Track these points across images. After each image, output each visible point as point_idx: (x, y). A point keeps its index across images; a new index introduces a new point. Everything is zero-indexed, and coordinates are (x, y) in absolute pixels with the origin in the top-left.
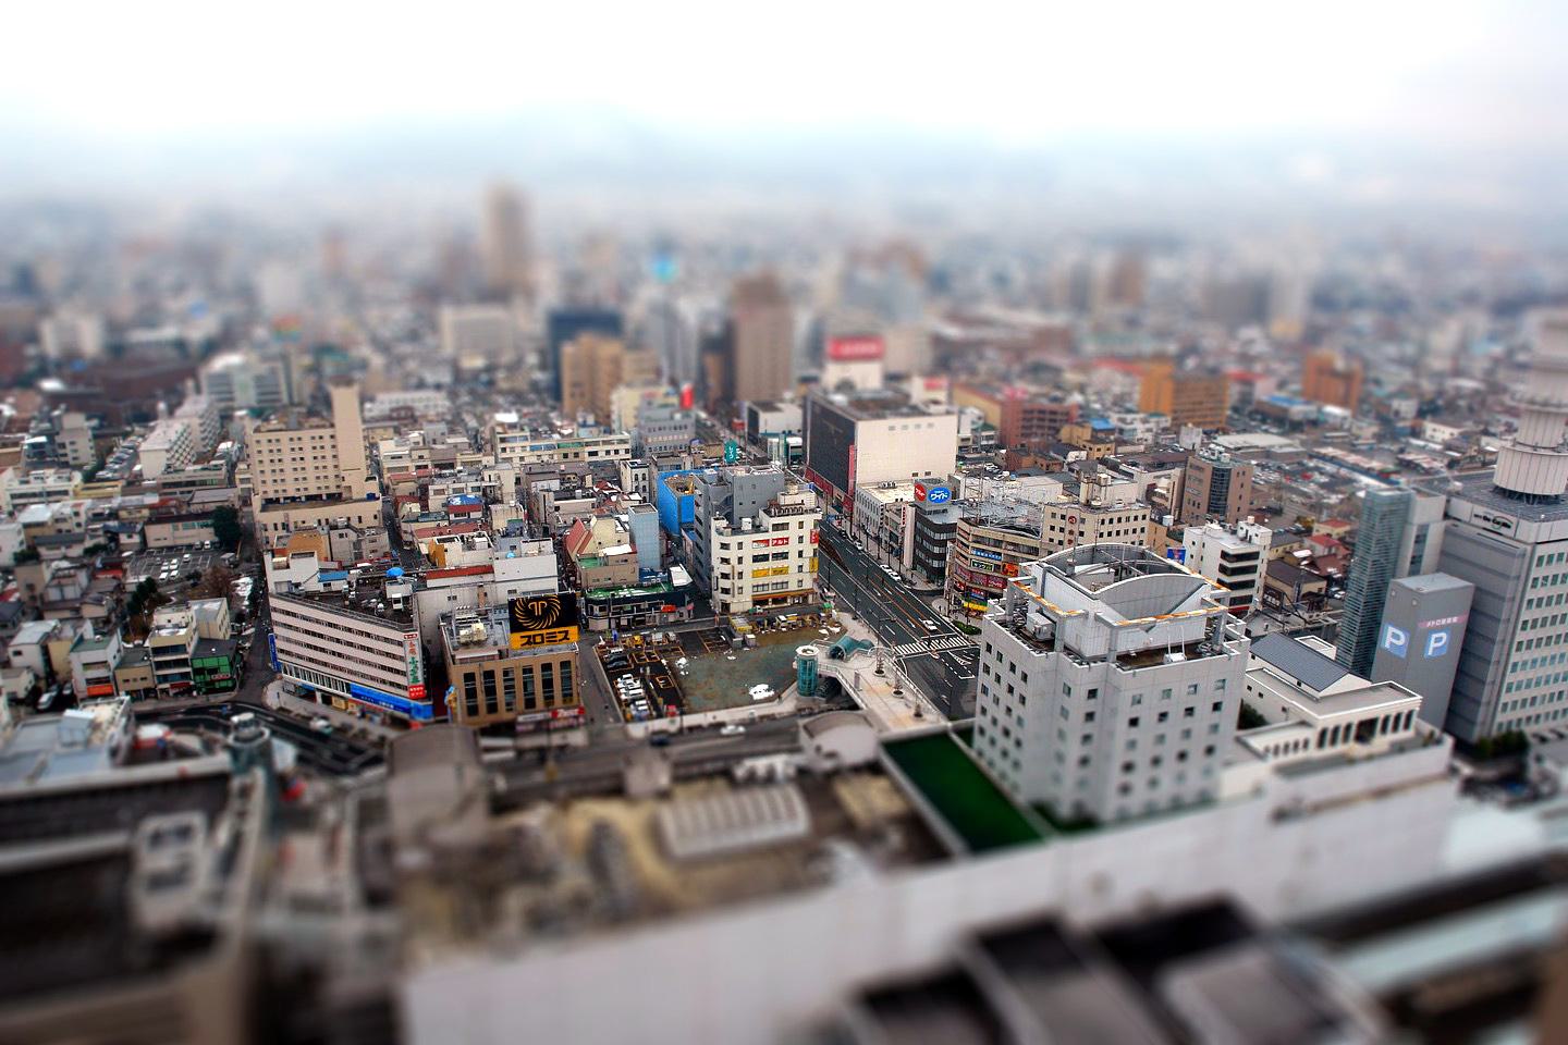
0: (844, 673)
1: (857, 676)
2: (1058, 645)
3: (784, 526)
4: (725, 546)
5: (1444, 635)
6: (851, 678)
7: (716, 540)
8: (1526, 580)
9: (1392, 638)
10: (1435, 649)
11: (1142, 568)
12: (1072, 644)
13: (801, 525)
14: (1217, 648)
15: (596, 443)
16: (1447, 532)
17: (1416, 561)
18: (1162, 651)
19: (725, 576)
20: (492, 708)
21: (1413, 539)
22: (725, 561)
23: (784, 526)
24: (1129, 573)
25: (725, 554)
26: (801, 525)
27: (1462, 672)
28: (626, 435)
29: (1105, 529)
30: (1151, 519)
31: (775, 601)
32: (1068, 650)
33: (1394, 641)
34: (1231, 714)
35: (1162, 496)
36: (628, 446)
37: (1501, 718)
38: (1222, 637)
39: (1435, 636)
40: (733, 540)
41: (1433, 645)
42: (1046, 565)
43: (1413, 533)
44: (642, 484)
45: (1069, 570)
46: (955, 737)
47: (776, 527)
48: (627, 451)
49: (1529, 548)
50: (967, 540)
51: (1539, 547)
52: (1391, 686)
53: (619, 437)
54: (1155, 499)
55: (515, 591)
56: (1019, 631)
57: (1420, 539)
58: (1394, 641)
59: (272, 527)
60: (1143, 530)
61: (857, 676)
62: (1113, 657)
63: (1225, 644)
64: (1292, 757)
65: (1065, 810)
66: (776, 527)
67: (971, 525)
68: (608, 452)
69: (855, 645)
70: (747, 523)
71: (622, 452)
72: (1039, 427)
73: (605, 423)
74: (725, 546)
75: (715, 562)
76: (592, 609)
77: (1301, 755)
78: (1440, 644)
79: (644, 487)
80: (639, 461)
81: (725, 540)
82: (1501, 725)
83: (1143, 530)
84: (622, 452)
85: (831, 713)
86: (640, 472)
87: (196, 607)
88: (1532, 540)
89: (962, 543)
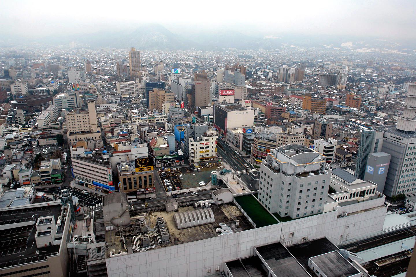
0: (224, 178)
1: (227, 179)
2: (281, 171)
3: (208, 140)
4: (192, 145)
5: (383, 168)
6: (226, 180)
7: (190, 143)
9: (369, 169)
12: (284, 171)
16: (384, 141)
17: (376, 149)
18: (308, 172)
19: (192, 153)
22: (192, 149)
23: (208, 140)
24: (300, 152)
25: (192, 147)
27: (388, 178)
28: (166, 115)
29: (293, 140)
31: (206, 159)
32: (283, 172)
33: (370, 170)
34: (327, 189)
36: (166, 118)
37: (398, 190)
38: (324, 169)
39: (381, 169)
40: (195, 143)
41: (380, 171)
45: (284, 151)
47: (206, 140)
48: (166, 120)
49: (406, 145)
52: (369, 182)
54: (306, 132)
55: (137, 157)
57: (377, 143)
58: (370, 170)
60: (303, 141)
61: (227, 179)
63: (325, 171)
64: (343, 201)
65: (282, 215)
66: (206, 140)
68: (161, 120)
69: (227, 171)
71: (165, 120)
74: (192, 145)
75: (190, 149)
77: (345, 200)
78: (382, 171)
80: (169, 122)
81: (192, 143)
83: (303, 141)
84: (165, 120)
86: (170, 125)
88: (406, 143)
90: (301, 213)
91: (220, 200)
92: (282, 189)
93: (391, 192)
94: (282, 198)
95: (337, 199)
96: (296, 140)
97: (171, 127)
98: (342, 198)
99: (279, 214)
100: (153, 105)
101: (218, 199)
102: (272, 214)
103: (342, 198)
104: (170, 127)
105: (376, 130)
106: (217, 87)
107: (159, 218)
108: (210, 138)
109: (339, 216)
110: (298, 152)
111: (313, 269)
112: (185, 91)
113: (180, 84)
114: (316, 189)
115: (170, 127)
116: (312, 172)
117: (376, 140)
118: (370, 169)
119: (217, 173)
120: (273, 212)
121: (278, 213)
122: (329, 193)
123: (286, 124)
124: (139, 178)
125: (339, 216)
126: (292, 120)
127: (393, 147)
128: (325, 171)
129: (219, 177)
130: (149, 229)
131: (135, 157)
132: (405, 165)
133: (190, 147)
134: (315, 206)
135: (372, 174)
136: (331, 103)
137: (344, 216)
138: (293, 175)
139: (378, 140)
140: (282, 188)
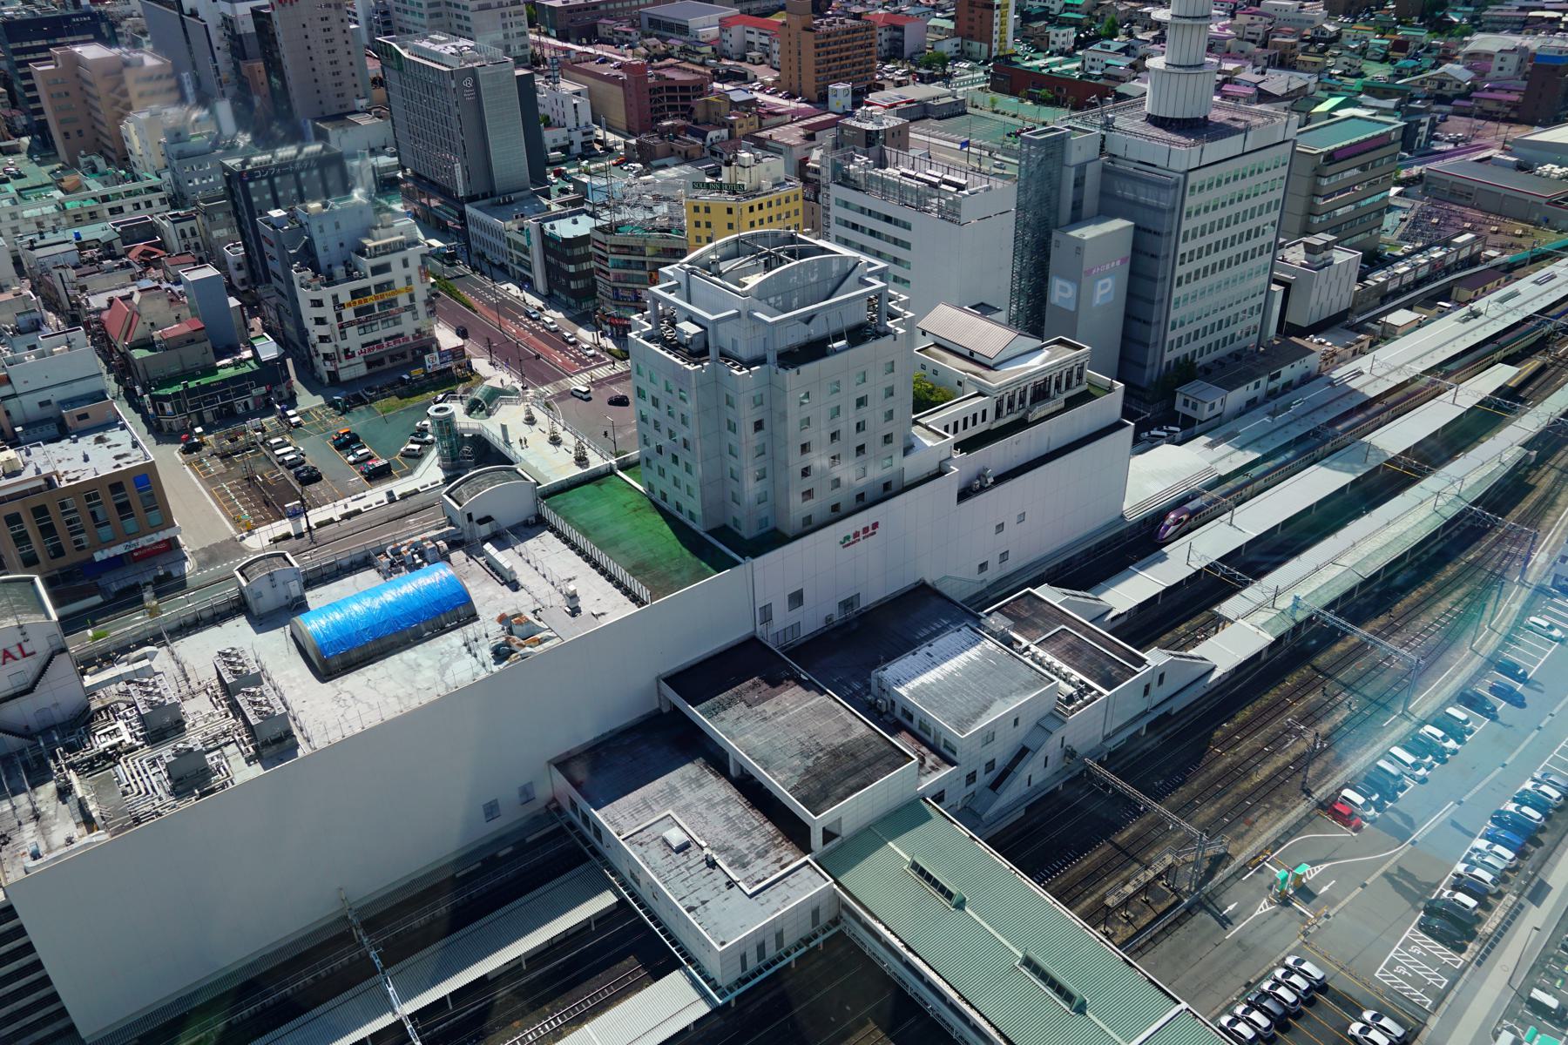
0: (490, 427)
1: (504, 428)
2: (713, 353)
3: (385, 268)
4: (318, 303)
5: (1109, 281)
6: (499, 434)
7: (304, 296)
8: (1177, 210)
9: (1060, 292)
10: (1102, 296)
11: (792, 254)
12: (728, 347)
13: (405, 263)
14: (882, 329)
15: (118, 196)
16: (1105, 170)
17: (1077, 205)
18: (826, 340)
19: (323, 339)
20: (58, 552)
21: (1072, 184)
22: (320, 321)
23: (385, 268)
24: (781, 262)
25: (318, 312)
26: (405, 263)
27: (1130, 317)
28: (155, 181)
29: (757, 215)
30: (804, 198)
31: (392, 359)
32: (725, 355)
33: (1063, 295)
34: (905, 398)
35: (816, 171)
36: (161, 195)
37: (1169, 356)
38: (884, 316)
39: (1100, 283)
40: (326, 294)
41: (1100, 292)
42: (687, 266)
43: (1070, 176)
44: (192, 241)
45: (713, 268)
46: (708, 537)
47: (376, 270)
48: (163, 201)
49: (1182, 176)
50: (605, 251)
51: (1191, 174)
52: (1060, 342)
53: (147, 183)
54: (810, 175)
55: (48, 402)
56: (673, 346)
57: (1079, 183)
58: (1063, 295)
59: (326, 27)
60: (797, 213)
61: (504, 428)
62: (772, 357)
63: (889, 324)
64: (972, 431)
65: (747, 531)
66: (376, 270)
67: (605, 233)
68: (137, 206)
69: (495, 395)
70: (339, 271)
71: (156, 203)
72: (671, 108)
73: (121, 158)
74: (318, 303)
75: (309, 324)
76: (162, 408)
77: (981, 427)
78: (1106, 291)
79: (197, 244)
80: (182, 212)
81: (316, 296)
82: (1169, 363)
83: (797, 213)
84: (156, 203)
85: (945, 902)
86: (186, 226)
87: (132, 127)
88: (1183, 168)
89: (600, 256)
90: (817, 506)
91: (481, 521)
92: (729, 428)
93: (1145, 367)
94: (733, 463)
95: (951, 428)
96: (774, 211)
97: (194, 234)
98: (970, 422)
99: (736, 529)
100: (73, 134)
101: (475, 518)
102: (708, 532)
103: (970, 422)
104: (188, 233)
105: (1074, 129)
106: (385, 13)
107: (227, 655)
108: (395, 259)
109: (965, 494)
110: (774, 265)
111: (893, 709)
112: (223, 45)
113: (194, 14)
114: (861, 402)
115: (188, 233)
116: (838, 337)
117: (1073, 170)
118: (1064, 289)
119: (456, 409)
120: (710, 527)
121: (732, 526)
122: (915, 412)
123: (717, 148)
124: (88, 498)
125: (965, 494)
126: (745, 128)
127: (1146, 196)
128: (889, 324)
129: (465, 422)
130: (188, 707)
131: (42, 404)
132: (1183, 255)
133: (308, 313)
134: (325, 228)
135: (1072, 308)
136: (897, 34)
137: (982, 489)
138: (761, 361)
139: (1081, 168)
140: (729, 421)
